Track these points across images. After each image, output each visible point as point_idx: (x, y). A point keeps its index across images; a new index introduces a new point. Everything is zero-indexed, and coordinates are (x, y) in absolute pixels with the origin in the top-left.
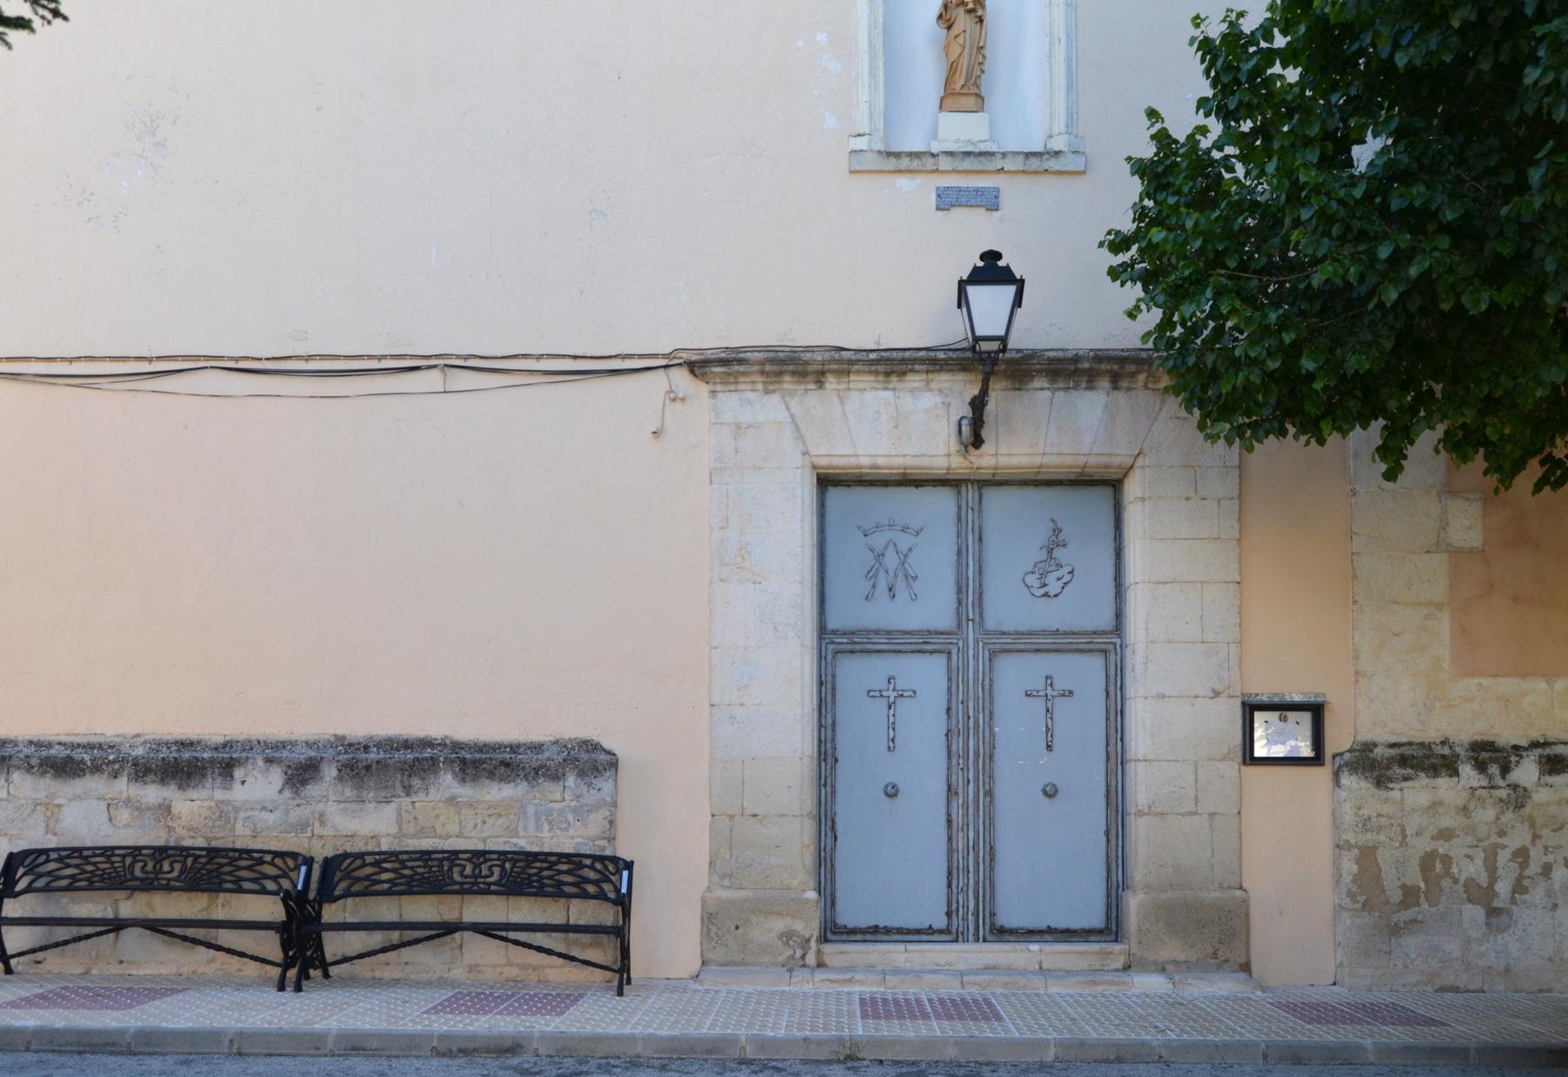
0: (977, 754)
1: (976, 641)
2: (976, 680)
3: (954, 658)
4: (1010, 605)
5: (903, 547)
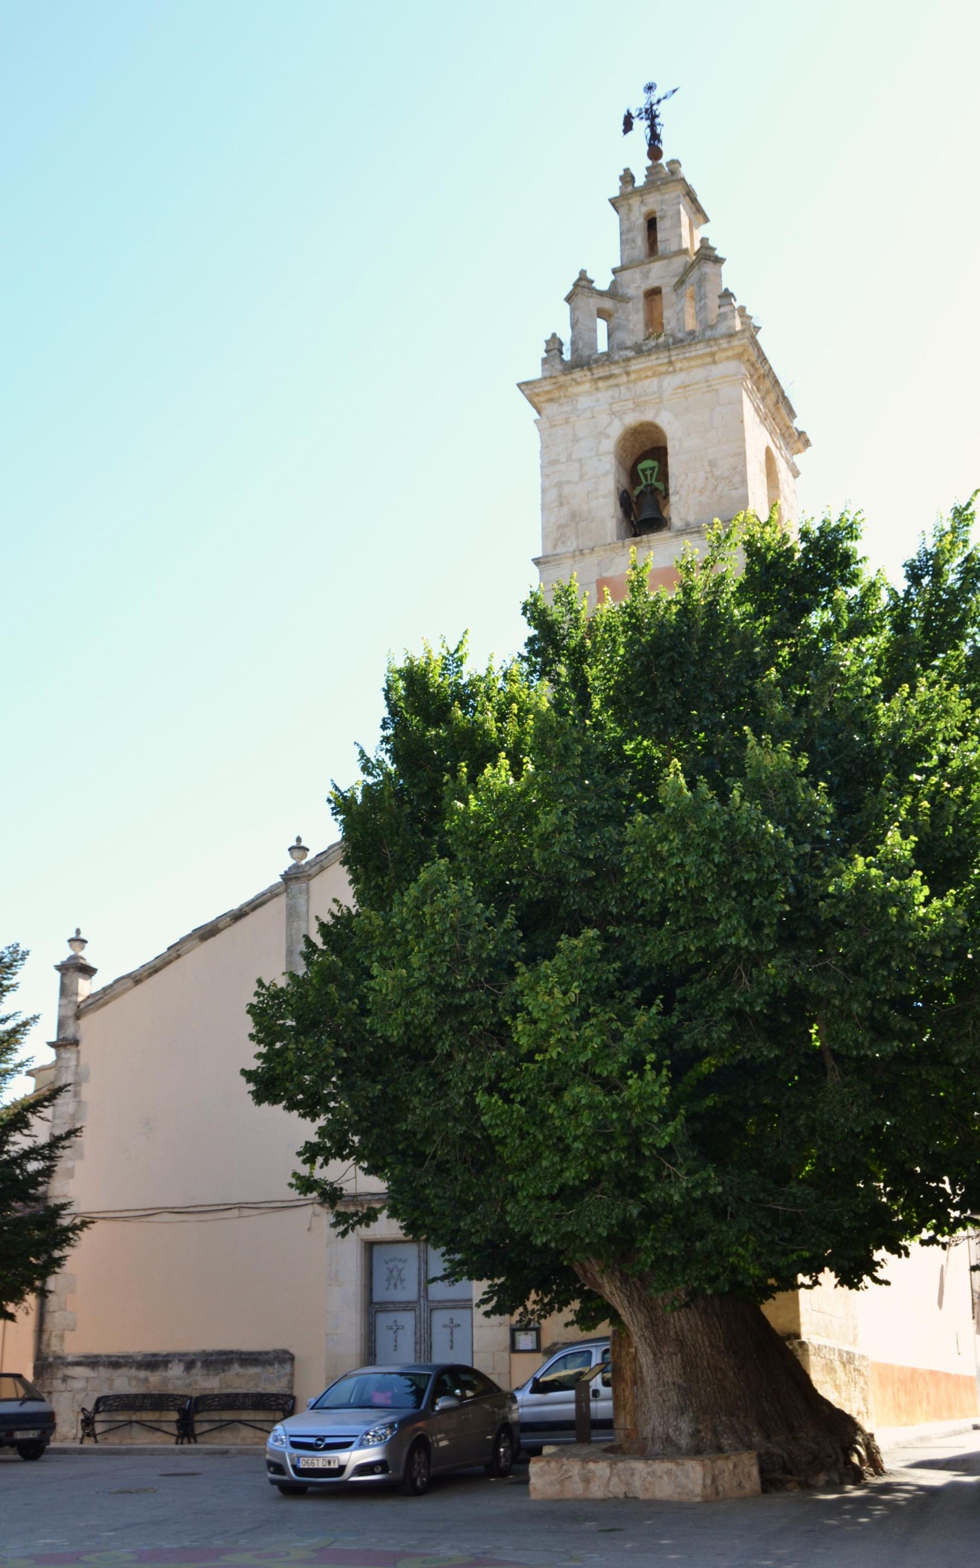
5: (400, 1268)
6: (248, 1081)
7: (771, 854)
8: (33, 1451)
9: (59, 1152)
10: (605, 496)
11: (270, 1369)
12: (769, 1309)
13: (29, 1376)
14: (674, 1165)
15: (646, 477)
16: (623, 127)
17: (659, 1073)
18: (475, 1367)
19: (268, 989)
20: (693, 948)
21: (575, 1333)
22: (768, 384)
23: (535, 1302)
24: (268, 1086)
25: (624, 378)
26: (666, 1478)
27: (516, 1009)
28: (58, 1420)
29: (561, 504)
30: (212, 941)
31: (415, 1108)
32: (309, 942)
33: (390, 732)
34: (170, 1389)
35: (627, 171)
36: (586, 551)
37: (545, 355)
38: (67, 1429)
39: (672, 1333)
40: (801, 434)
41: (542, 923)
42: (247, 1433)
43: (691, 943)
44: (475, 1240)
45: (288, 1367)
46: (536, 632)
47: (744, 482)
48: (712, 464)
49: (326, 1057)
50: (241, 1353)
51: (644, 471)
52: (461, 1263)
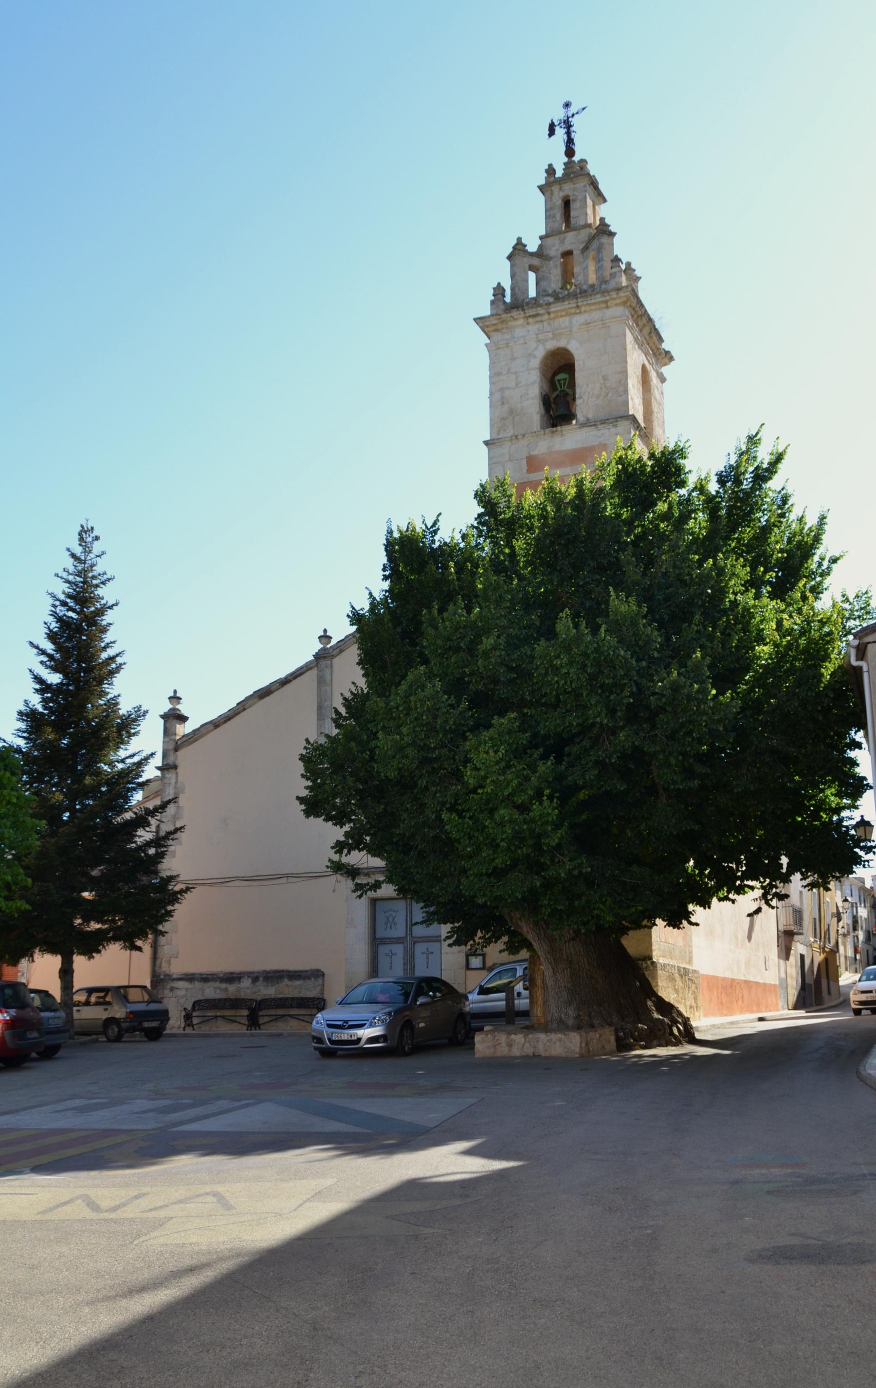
6: (301, 804)
7: (622, 668)
8: (154, 1035)
9: (170, 842)
10: (533, 399)
11: (308, 982)
12: (630, 943)
13: (149, 986)
14: (562, 855)
15: (560, 385)
16: (548, 132)
17: (552, 801)
18: (443, 978)
19: (312, 745)
20: (575, 724)
21: (506, 957)
22: (644, 320)
23: (480, 938)
24: (313, 806)
25: (547, 317)
26: (558, 1043)
27: (467, 761)
28: (171, 1014)
29: (503, 403)
30: (267, 699)
31: (404, 819)
32: (337, 712)
33: (387, 573)
34: (242, 995)
35: (550, 166)
36: (519, 437)
37: (493, 298)
38: (175, 1022)
39: (565, 956)
40: (667, 353)
41: (486, 704)
42: (293, 1023)
43: (573, 719)
44: (441, 900)
45: (320, 980)
46: (483, 510)
47: (626, 391)
48: (605, 378)
49: (349, 789)
50: (290, 971)
51: (559, 381)
52: (434, 913)
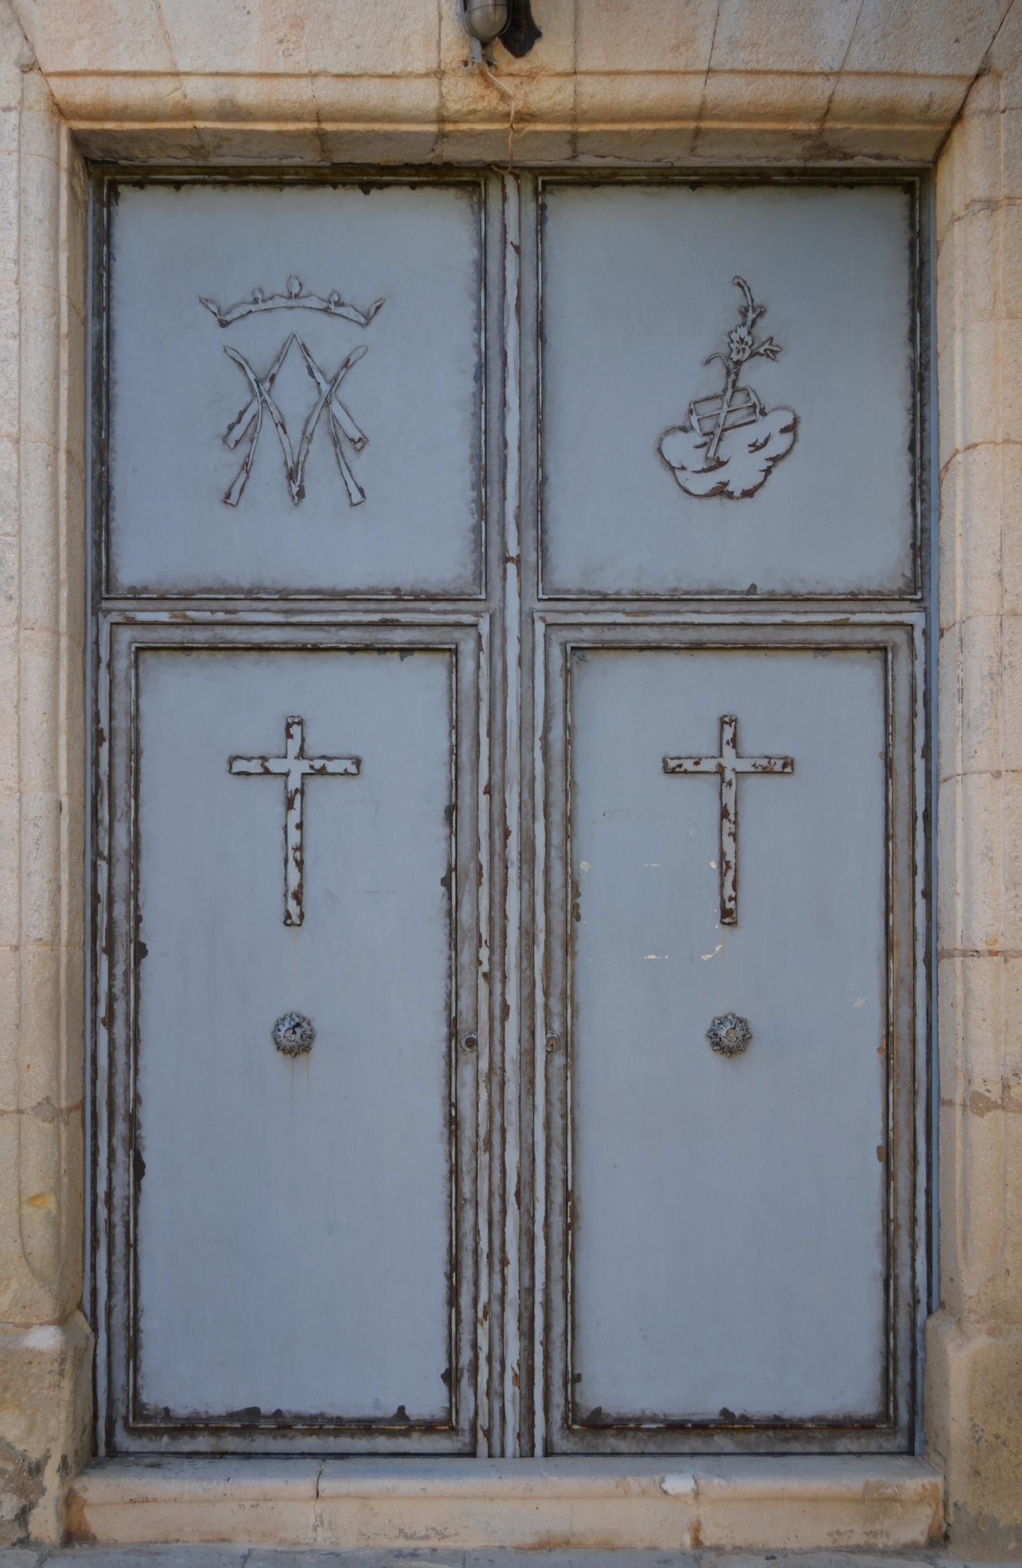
0: (528, 934)
1: (527, 619)
2: (525, 727)
3: (467, 666)
4: (622, 523)
5: (328, 355)
